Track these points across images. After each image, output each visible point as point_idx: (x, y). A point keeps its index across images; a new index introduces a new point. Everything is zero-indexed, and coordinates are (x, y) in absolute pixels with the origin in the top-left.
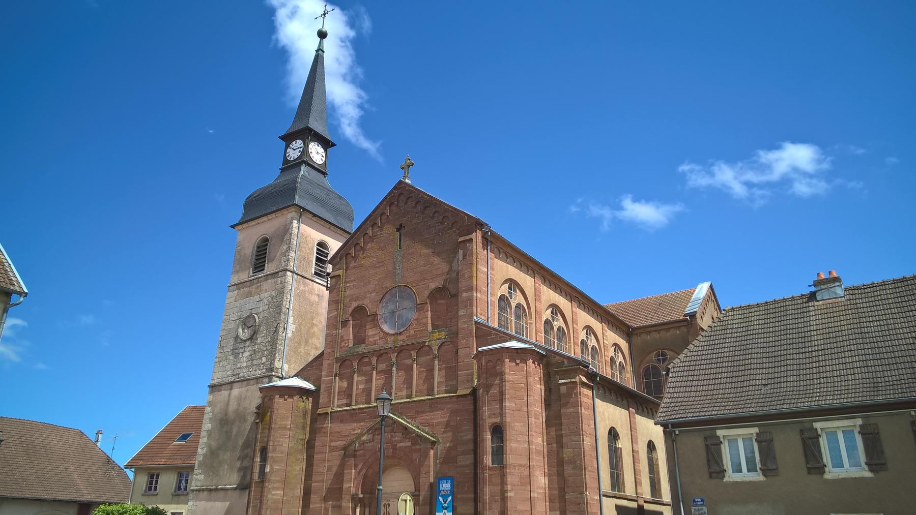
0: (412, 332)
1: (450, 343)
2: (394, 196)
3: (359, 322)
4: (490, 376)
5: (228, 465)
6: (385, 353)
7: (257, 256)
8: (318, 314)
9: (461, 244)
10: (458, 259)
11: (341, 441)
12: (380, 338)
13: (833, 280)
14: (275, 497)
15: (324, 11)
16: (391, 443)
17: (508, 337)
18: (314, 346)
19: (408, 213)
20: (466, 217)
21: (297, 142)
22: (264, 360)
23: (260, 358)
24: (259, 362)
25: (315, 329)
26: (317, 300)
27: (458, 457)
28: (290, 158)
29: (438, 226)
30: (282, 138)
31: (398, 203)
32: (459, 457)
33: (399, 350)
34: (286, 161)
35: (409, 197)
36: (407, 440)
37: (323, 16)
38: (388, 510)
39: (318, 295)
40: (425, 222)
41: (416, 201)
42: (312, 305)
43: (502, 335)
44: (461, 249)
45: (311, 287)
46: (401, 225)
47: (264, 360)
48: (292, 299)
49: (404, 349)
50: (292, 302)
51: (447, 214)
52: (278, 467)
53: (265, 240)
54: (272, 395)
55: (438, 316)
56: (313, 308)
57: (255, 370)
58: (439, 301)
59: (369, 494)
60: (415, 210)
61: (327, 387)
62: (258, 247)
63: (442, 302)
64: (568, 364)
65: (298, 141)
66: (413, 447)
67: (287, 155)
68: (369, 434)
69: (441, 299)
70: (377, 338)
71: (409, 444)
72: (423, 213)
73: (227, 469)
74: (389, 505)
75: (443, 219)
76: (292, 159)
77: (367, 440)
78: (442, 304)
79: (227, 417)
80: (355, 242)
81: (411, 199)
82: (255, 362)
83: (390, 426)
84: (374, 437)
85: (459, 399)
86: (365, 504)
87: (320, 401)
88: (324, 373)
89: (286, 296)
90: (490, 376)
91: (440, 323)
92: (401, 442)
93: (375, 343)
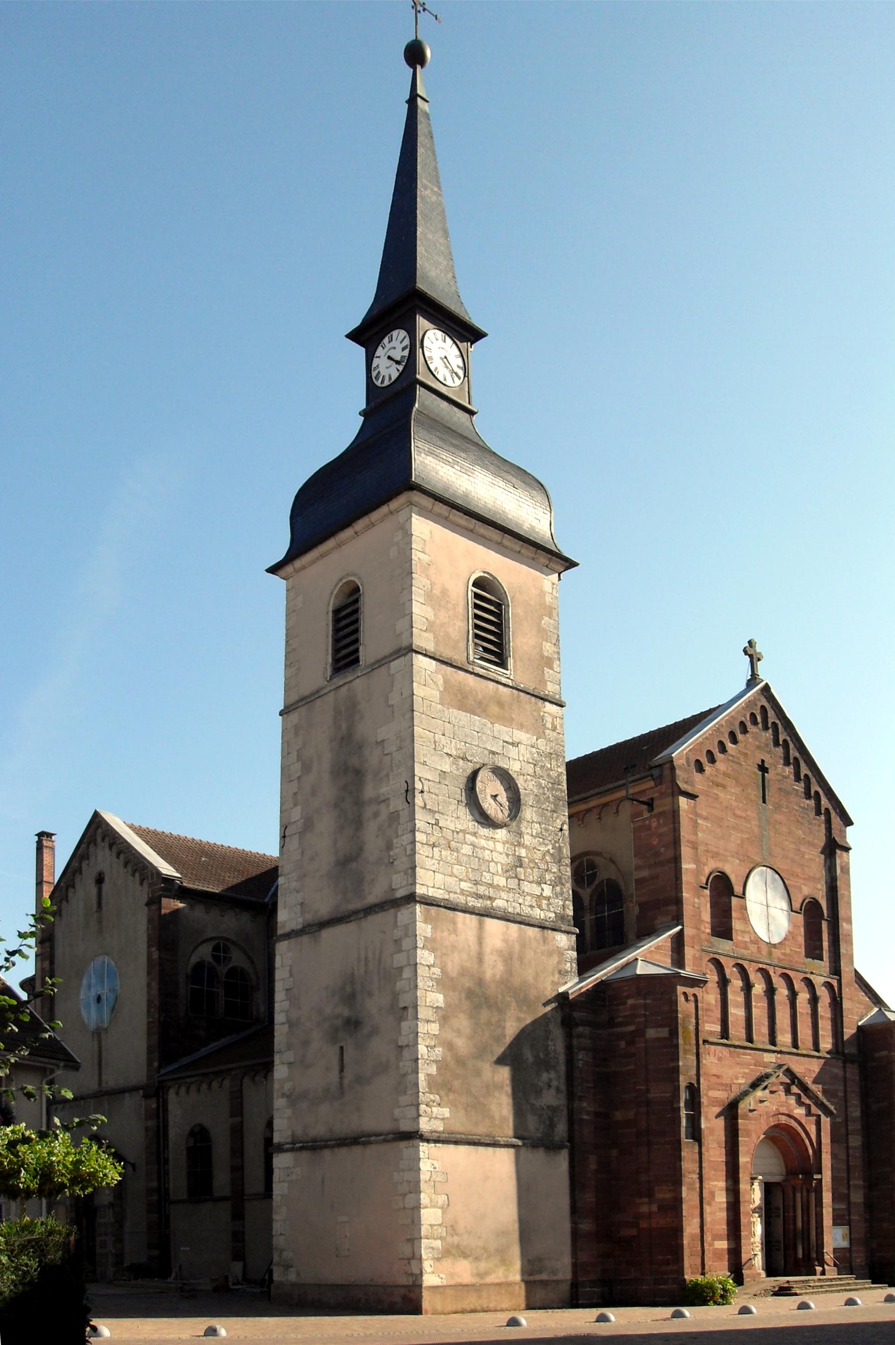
24: (537, 890)
28: (382, 382)
62: (336, 612)
65: (395, 333)
67: (374, 374)
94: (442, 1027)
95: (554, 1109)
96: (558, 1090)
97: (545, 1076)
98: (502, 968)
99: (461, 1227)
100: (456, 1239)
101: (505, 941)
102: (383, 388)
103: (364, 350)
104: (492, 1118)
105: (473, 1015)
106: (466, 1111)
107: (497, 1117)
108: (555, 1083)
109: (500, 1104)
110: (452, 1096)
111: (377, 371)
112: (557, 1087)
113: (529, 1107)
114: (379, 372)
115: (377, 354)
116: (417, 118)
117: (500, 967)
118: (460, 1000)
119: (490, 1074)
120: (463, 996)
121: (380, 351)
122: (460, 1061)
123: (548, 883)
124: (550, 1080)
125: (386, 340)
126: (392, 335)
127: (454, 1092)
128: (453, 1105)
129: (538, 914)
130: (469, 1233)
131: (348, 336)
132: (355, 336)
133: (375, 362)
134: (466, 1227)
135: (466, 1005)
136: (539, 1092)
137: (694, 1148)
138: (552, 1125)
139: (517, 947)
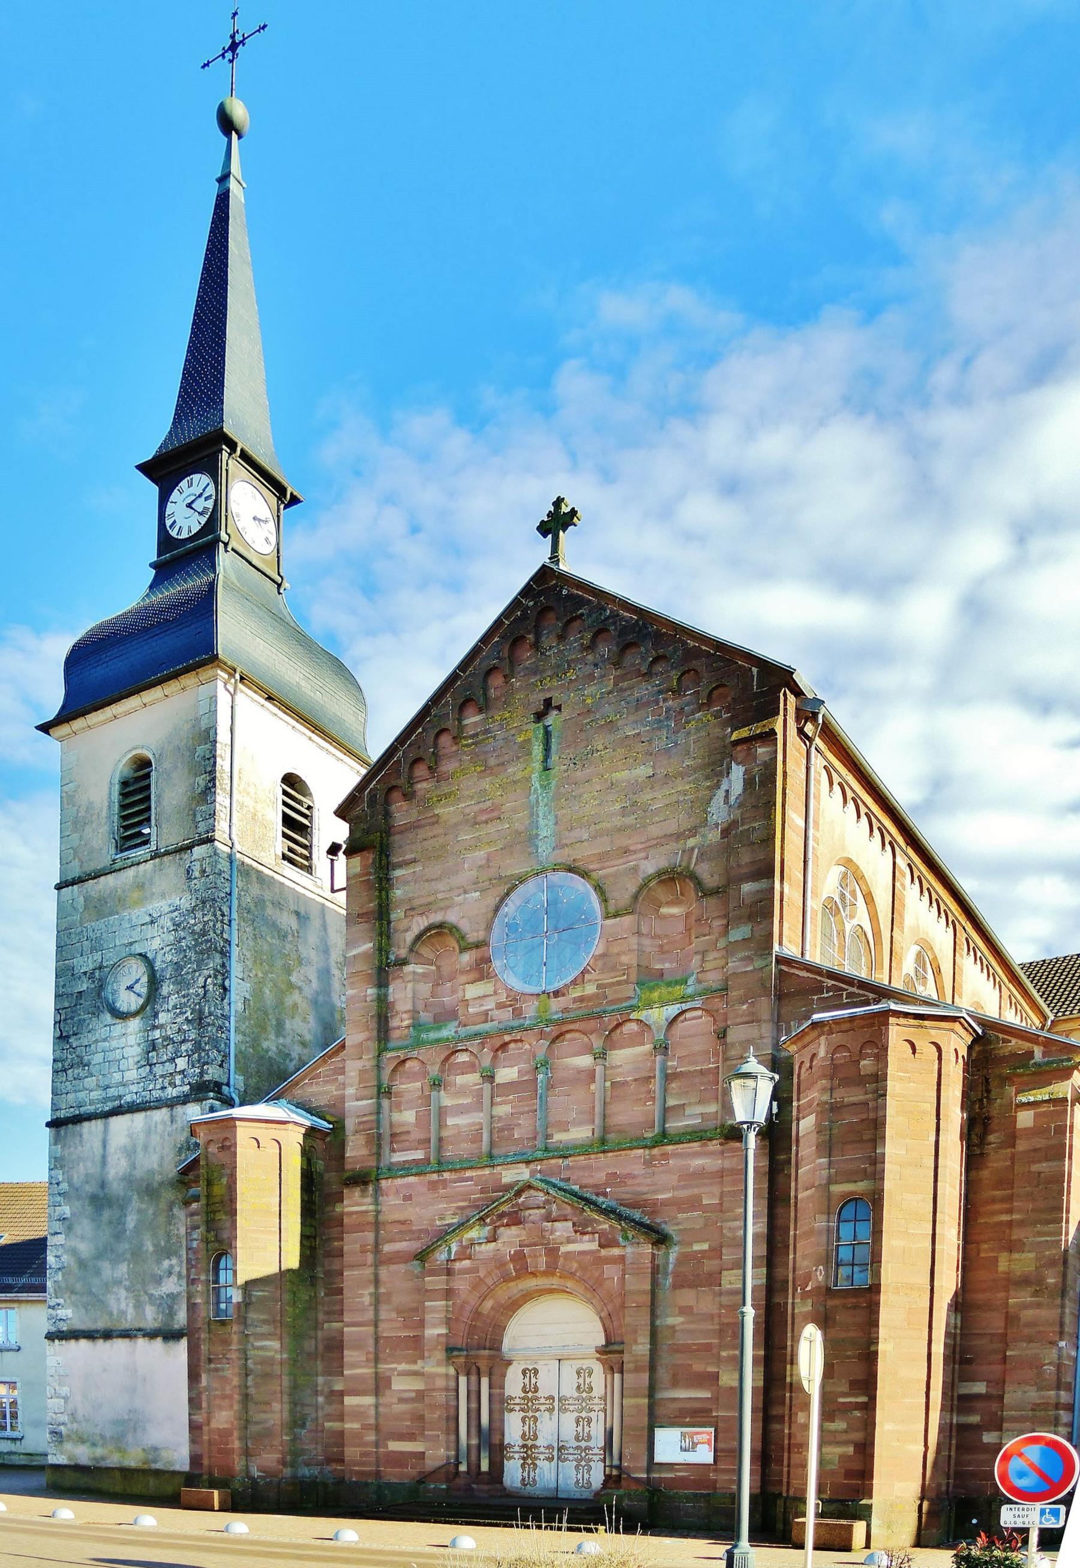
0: (590, 989)
1: (699, 1013)
2: (524, 617)
3: (433, 968)
4: (839, 1085)
5: (127, 1289)
6: (516, 1041)
7: (123, 807)
8: (300, 961)
9: (739, 748)
10: (727, 791)
11: (409, 1240)
12: (500, 1006)
13: (30, 1288)
14: (261, 1353)
15: (233, 37)
16: (542, 1244)
17: (871, 996)
18: (297, 1038)
19: (569, 666)
20: (755, 670)
21: (195, 483)
22: (182, 1063)
23: (172, 1060)
24: (169, 1068)
25: (296, 997)
26: (295, 926)
27: (725, 1273)
28: (179, 532)
29: (665, 700)
30: (146, 469)
31: (538, 636)
32: (725, 1273)
33: (554, 1034)
34: (166, 541)
35: (573, 619)
36: (586, 1237)
37: (229, 55)
38: (533, 1380)
39: (297, 913)
40: (622, 690)
41: (596, 629)
42: (285, 936)
43: (855, 990)
44: (738, 764)
45: (277, 890)
46: (548, 703)
47: (182, 1063)
48: (235, 915)
49: (568, 1032)
50: (234, 924)
51: (695, 664)
52: (261, 1293)
53: (143, 765)
54: (226, 1139)
55: (661, 946)
56: (288, 946)
57: (163, 1088)
58: (664, 910)
59: (490, 1349)
60: (590, 657)
61: (360, 1123)
62: (125, 784)
63: (675, 910)
64: (1044, 1057)
65: (196, 477)
66: (604, 1252)
67: (168, 523)
68: (486, 1225)
69: (670, 904)
70: (489, 1004)
71: (594, 1246)
72: (617, 664)
73: (126, 1298)
74: (536, 1372)
75: (679, 679)
76: (184, 535)
77: (479, 1238)
78: (673, 916)
79: (106, 1191)
80: (412, 756)
81: (577, 624)
82: (159, 1070)
83: (539, 1208)
84: (498, 1232)
85: (727, 1146)
86: (478, 1369)
87: (347, 1155)
88: (350, 1091)
89: (220, 910)
90: (839, 1085)
91: (667, 965)
92: (569, 1241)
93: (485, 1016)
94: (67, 1235)
95: (172, 1297)
96: (180, 1276)
97: (166, 1263)
98: (125, 1164)
99: (80, 1414)
100: (75, 1426)
101: (130, 1136)
102: (177, 539)
103: (348, 825)
104: (111, 1314)
105: (95, 1219)
106: (86, 1309)
107: (115, 1312)
108: (177, 1269)
109: (119, 1300)
110: (74, 1298)
111: (173, 519)
112: (179, 1272)
113: (147, 1298)
114: (175, 522)
115: (172, 498)
116: (260, 311)
117: (124, 1163)
118: (83, 1206)
119: (109, 1272)
120: (87, 1202)
121: (175, 495)
122: (82, 1264)
123: (184, 1054)
124: (172, 1266)
125: (184, 484)
126: (192, 479)
127: (76, 1294)
128: (75, 1305)
129: (171, 1092)
130: (88, 1421)
131: (139, 467)
132: (146, 469)
133: (170, 508)
134: (84, 1416)
135: (89, 1209)
136: (158, 1280)
137: (371, 901)
138: (171, 1314)
139: (142, 1136)
